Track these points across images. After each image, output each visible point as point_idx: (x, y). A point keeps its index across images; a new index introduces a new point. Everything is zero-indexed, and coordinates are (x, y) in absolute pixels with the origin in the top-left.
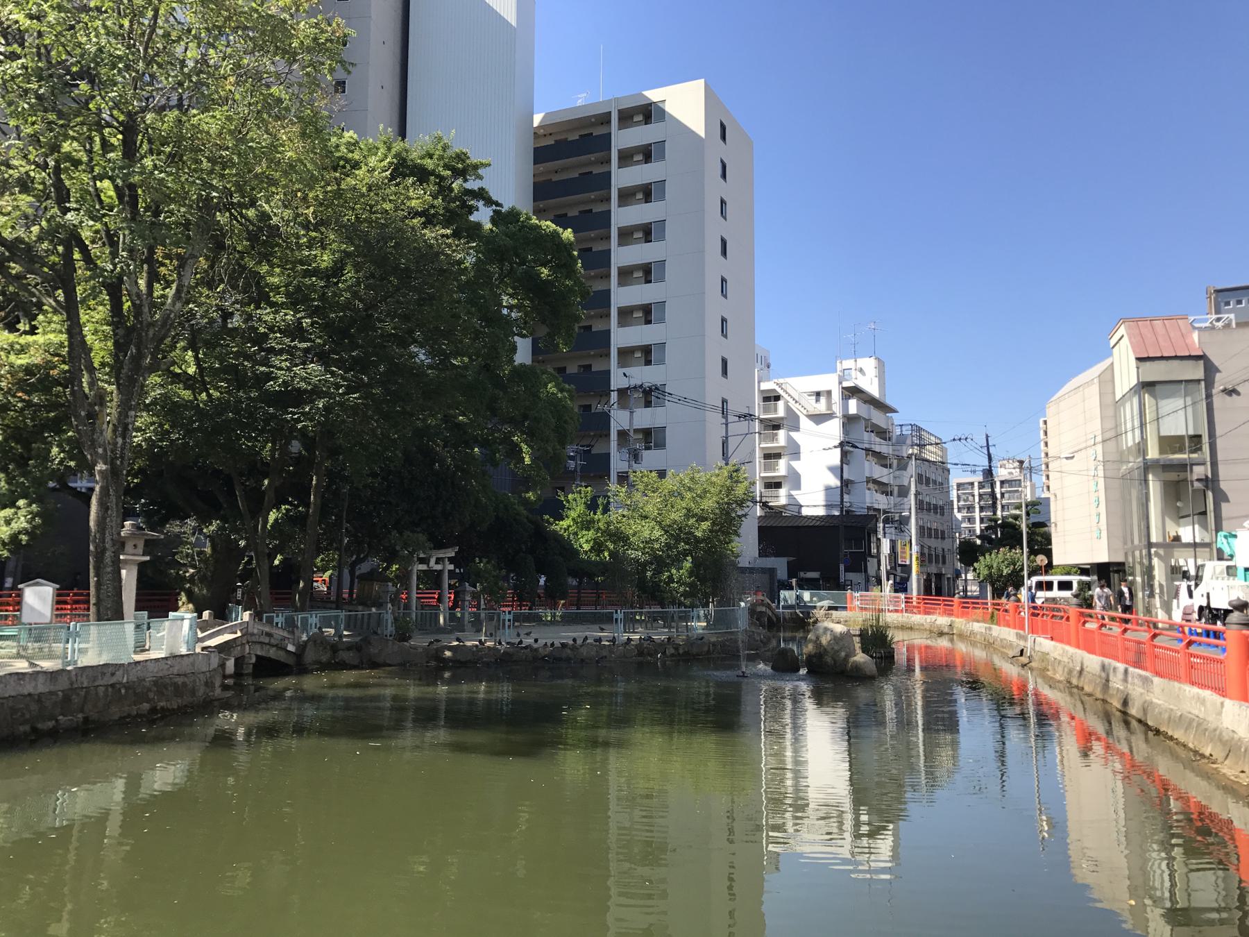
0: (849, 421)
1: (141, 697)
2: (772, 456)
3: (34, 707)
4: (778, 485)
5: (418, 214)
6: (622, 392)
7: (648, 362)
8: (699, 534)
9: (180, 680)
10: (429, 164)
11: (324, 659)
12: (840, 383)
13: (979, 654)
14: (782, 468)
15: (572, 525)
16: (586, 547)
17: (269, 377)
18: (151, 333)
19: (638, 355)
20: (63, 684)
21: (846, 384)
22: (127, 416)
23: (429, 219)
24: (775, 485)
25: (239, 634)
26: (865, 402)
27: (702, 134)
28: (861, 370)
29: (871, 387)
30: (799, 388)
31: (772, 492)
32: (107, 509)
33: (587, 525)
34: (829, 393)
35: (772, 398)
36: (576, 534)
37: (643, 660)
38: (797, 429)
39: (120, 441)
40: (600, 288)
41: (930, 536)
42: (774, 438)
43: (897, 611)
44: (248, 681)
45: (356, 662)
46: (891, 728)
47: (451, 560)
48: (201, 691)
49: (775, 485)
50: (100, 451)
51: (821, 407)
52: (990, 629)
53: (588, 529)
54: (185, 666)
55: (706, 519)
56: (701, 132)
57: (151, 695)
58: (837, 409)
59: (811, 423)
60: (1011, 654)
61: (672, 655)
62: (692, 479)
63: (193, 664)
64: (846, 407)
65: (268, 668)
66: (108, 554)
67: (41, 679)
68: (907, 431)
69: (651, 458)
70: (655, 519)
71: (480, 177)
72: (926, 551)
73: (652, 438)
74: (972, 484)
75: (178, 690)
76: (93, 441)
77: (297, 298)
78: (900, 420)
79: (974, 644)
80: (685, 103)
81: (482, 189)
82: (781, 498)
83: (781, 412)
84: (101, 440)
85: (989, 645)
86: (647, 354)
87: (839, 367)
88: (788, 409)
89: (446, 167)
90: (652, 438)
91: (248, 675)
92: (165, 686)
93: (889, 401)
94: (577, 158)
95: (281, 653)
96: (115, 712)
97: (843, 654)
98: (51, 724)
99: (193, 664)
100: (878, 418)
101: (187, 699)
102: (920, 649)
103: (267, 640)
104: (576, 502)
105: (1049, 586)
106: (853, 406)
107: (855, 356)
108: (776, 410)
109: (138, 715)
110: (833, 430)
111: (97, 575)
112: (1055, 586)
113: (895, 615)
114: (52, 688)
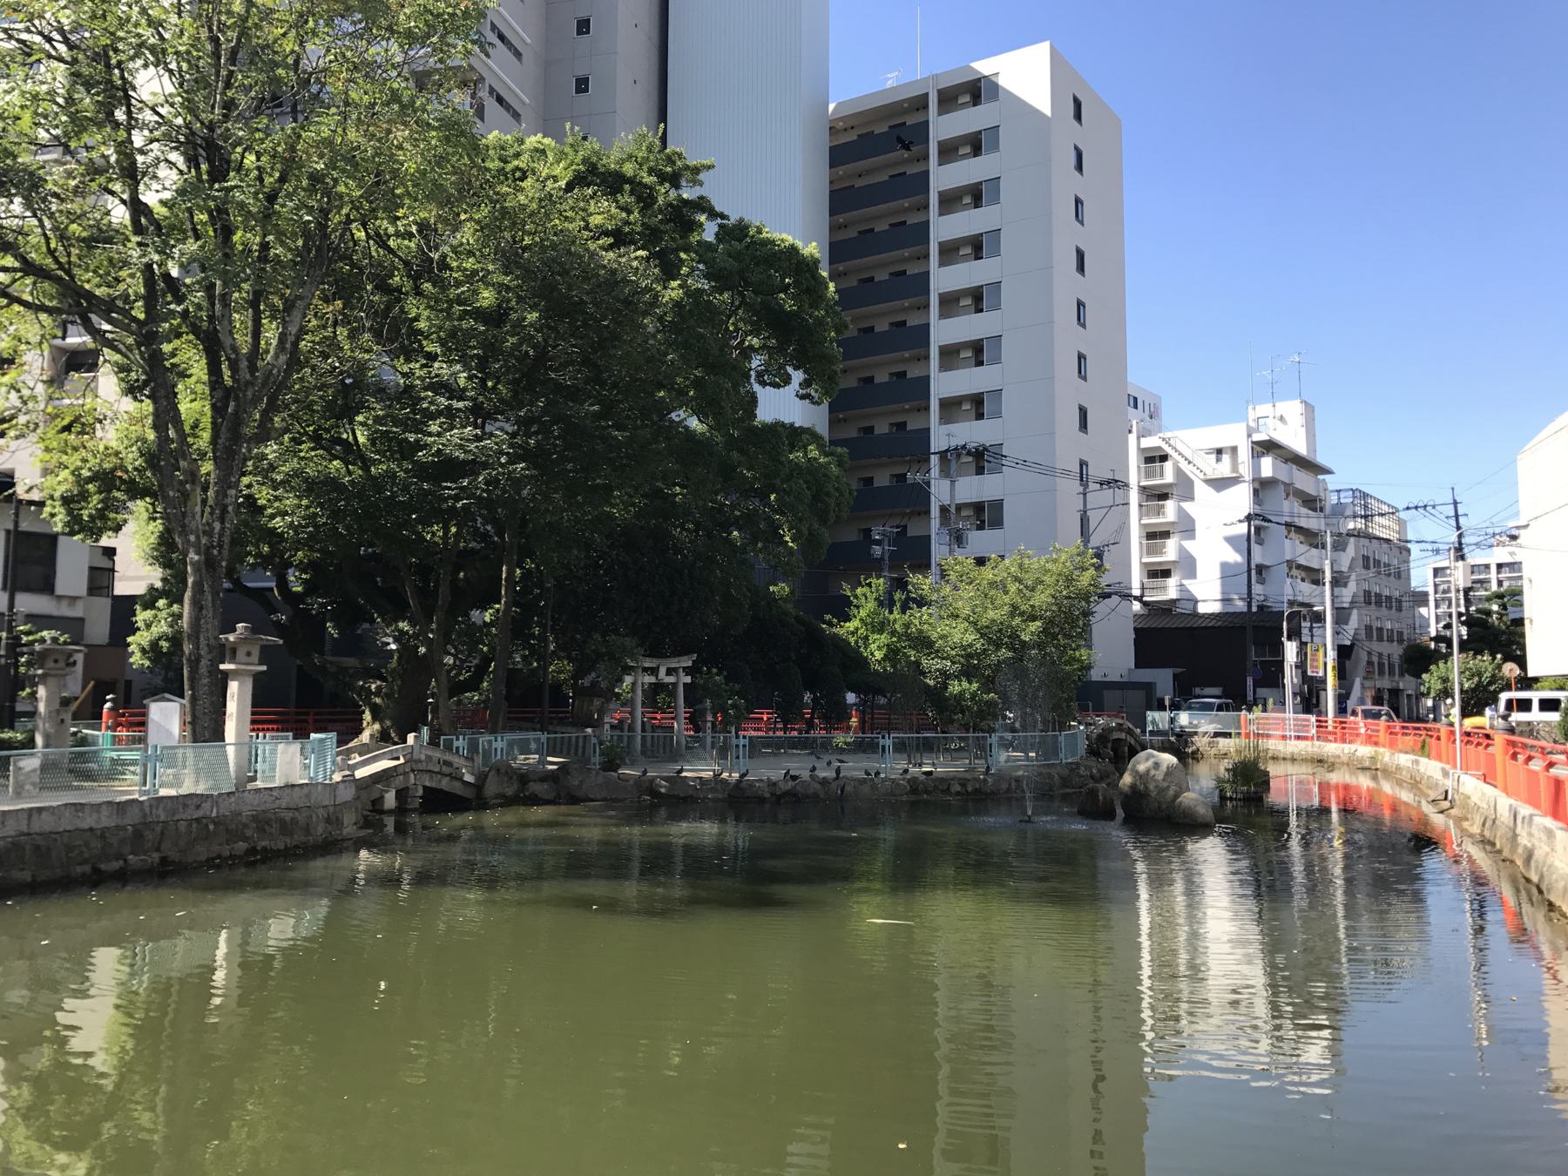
0: (1262, 487)
1: (235, 834)
2: (1156, 536)
3: (96, 844)
4: (1166, 574)
5: (607, 234)
6: (943, 455)
7: (980, 416)
8: (1026, 637)
9: (288, 816)
10: (629, 169)
11: (510, 791)
12: (1249, 436)
13: (1406, 796)
14: (1170, 551)
15: (865, 626)
16: (879, 655)
17: (418, 446)
18: (249, 394)
19: (966, 406)
20: (132, 818)
21: (1257, 437)
22: (226, 496)
23: (620, 238)
24: (1160, 573)
25: (402, 761)
26: (1286, 461)
27: (1048, 112)
28: (1282, 418)
29: (1294, 439)
30: (1192, 444)
31: (1159, 581)
32: (201, 608)
33: (880, 628)
34: (1234, 450)
35: (1155, 458)
36: (866, 638)
37: (923, 798)
38: (1190, 497)
39: (217, 526)
40: (916, 322)
41: (1380, 639)
42: (1159, 511)
43: (1306, 738)
44: (414, 818)
45: (551, 796)
46: (1300, 899)
47: (688, 671)
48: (320, 829)
49: (1160, 573)
50: (192, 538)
51: (1224, 469)
52: (1417, 762)
53: (881, 631)
54: (297, 798)
55: (1033, 618)
56: (1045, 107)
57: (248, 833)
58: (1245, 470)
59: (1211, 490)
60: (1433, 795)
61: (958, 793)
62: (1021, 566)
63: (308, 796)
64: (1256, 468)
65: (438, 802)
66: (204, 662)
67: (105, 811)
68: (1346, 499)
69: (980, 541)
70: (967, 619)
71: (696, 183)
72: (1375, 659)
73: (987, 514)
74: (1487, 567)
75: (286, 828)
76: (184, 526)
77: (455, 344)
78: (1336, 484)
79: (1400, 783)
80: (1025, 74)
81: (701, 198)
82: (1170, 590)
83: (1169, 477)
84: (193, 525)
85: (1415, 784)
86: (977, 405)
87: (1252, 415)
88: (1179, 472)
89: (651, 171)
90: (987, 514)
91: (414, 810)
92: (268, 823)
93: (1321, 459)
94: (884, 160)
95: (457, 784)
96: (202, 852)
97: (1171, 792)
98: (116, 865)
99: (308, 796)
100: (1303, 481)
101: (299, 838)
102: (1337, 786)
103: (446, 769)
104: (866, 597)
105: (1525, 705)
106: (1267, 466)
107: (1273, 399)
108: (1162, 475)
109: (231, 857)
110: (1240, 500)
111: (192, 688)
112: (1535, 705)
113: (1302, 744)
114: (120, 822)
